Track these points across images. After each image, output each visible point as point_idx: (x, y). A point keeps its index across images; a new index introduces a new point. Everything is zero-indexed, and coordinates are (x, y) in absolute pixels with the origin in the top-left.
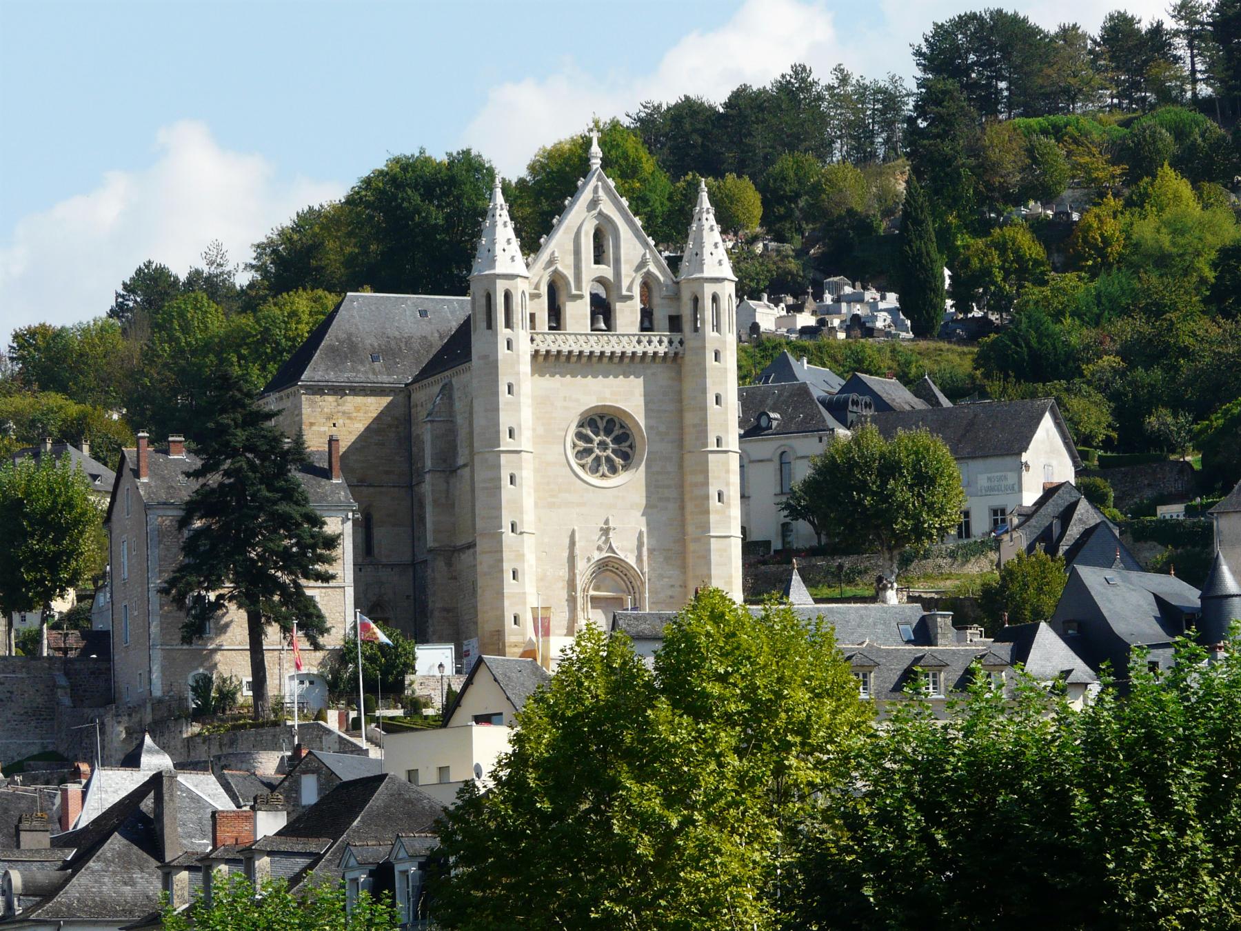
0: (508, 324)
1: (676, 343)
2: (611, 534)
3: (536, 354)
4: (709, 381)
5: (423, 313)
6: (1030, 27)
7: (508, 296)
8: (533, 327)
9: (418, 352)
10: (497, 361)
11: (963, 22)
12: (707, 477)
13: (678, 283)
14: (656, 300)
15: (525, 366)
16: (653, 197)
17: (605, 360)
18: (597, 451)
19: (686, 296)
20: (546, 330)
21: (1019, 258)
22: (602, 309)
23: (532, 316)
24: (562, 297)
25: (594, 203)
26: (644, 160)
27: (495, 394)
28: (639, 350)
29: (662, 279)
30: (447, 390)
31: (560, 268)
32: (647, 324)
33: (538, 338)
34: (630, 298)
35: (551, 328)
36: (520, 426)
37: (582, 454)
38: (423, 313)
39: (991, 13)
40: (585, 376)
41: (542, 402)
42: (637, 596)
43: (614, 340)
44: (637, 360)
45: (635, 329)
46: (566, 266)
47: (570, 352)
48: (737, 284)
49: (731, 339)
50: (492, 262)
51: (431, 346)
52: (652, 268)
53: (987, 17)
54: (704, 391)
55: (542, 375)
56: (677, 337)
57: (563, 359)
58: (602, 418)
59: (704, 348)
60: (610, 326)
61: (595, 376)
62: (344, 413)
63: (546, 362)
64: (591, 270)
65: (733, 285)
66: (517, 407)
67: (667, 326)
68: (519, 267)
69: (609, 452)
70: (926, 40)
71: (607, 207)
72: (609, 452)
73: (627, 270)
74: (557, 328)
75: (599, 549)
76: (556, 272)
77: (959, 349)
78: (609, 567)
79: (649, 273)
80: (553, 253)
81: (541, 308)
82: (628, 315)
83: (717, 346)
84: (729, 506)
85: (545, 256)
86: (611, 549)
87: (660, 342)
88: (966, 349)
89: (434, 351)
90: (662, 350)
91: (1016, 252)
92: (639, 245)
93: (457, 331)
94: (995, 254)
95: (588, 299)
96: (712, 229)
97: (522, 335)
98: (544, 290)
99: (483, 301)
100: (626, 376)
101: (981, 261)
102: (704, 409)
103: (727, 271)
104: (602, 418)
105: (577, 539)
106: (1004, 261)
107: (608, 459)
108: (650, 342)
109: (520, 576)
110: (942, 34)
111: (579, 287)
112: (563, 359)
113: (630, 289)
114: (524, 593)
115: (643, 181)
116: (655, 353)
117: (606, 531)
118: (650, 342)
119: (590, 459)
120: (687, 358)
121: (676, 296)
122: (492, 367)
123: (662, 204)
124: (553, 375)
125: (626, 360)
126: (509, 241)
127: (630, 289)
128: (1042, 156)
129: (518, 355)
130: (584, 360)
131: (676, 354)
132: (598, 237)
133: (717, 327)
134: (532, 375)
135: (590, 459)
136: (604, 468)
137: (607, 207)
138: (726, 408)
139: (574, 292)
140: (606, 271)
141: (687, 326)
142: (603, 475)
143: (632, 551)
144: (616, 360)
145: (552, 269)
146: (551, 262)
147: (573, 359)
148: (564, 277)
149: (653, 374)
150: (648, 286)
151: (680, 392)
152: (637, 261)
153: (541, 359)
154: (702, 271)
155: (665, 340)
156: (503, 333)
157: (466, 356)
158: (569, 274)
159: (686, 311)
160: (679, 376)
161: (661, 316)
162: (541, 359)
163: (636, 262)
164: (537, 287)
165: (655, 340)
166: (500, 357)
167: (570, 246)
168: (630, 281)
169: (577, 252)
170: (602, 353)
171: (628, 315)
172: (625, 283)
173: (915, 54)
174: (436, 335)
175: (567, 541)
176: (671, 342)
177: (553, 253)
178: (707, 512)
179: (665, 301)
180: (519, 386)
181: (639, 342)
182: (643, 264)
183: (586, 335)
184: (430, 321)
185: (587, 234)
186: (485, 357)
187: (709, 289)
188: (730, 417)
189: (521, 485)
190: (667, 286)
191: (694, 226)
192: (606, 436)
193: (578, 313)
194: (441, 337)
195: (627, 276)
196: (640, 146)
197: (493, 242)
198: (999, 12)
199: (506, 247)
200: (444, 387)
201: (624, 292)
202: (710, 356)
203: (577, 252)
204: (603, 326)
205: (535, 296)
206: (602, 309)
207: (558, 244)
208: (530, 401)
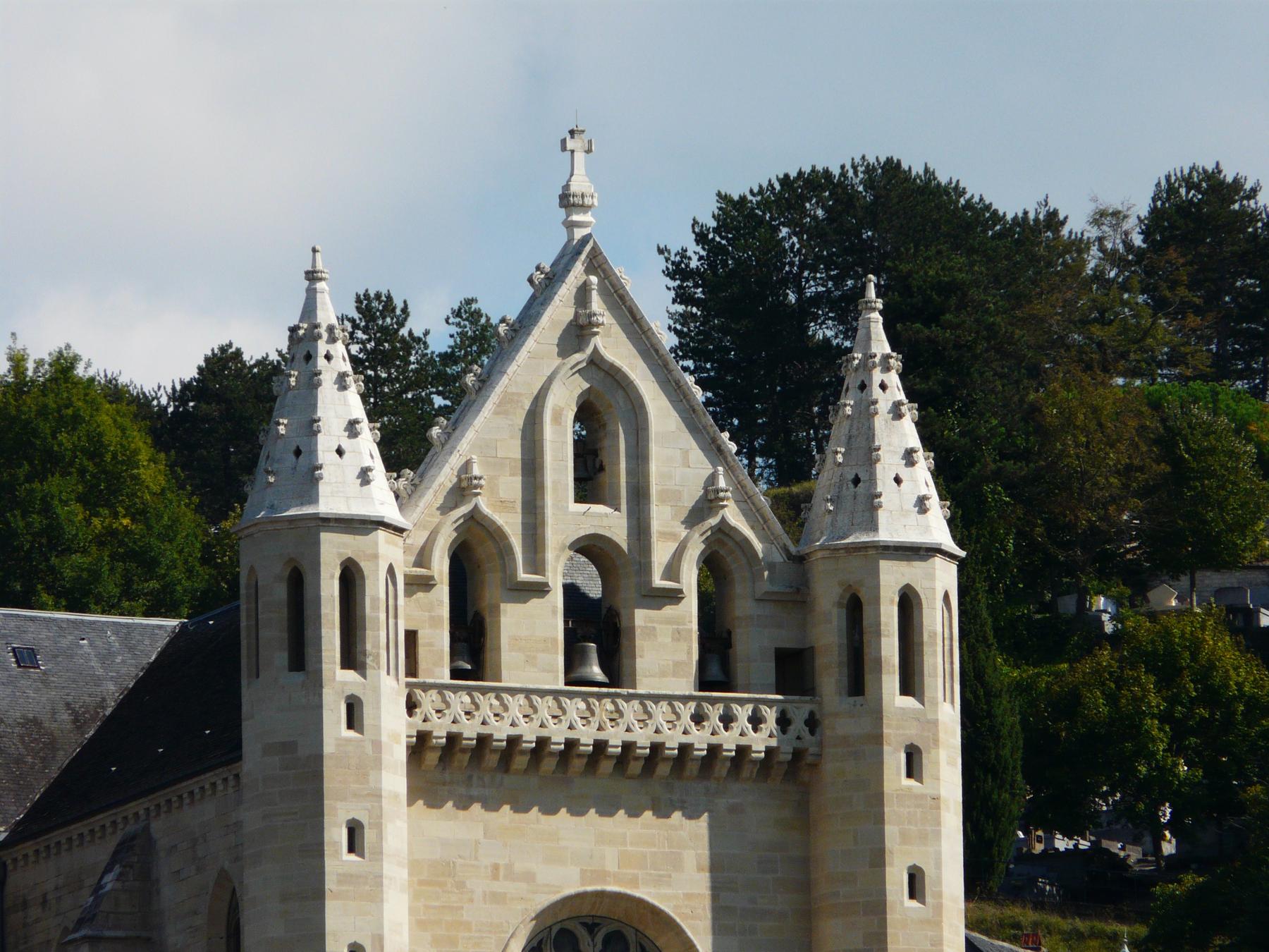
0: (352, 658)
1: (798, 726)
3: (419, 745)
4: (891, 831)
5: (26, 658)
6: (969, 205)
7: (351, 577)
8: (412, 670)
9: (19, 761)
10: (319, 758)
11: (796, 192)
13: (801, 559)
14: (743, 606)
15: (394, 779)
16: (170, 553)
17: (606, 766)
19: (827, 595)
20: (446, 678)
21: (1212, 695)
22: (597, 632)
23: (411, 637)
24: (491, 589)
26: (143, 457)
27: (315, 850)
28: (700, 739)
29: (758, 546)
30: (135, 854)
31: (486, 509)
32: (715, 671)
33: (428, 701)
34: (674, 596)
35: (456, 673)
38: (26, 658)
39: (869, 170)
40: (550, 810)
41: (434, 877)
43: (631, 710)
44: (692, 768)
45: (685, 684)
46: (503, 505)
47: (513, 741)
48: (962, 565)
49: (948, 715)
50: (309, 480)
51: (52, 745)
52: (733, 515)
53: (857, 182)
54: (878, 859)
55: (434, 802)
56: (800, 710)
57: (492, 760)
58: (591, 928)
59: (877, 739)
60: (617, 671)
61: (578, 811)
63: (452, 769)
64: (567, 518)
65: (953, 568)
66: (373, 888)
67: (772, 678)
68: (379, 499)
70: (701, 238)
73: (665, 520)
74: (477, 674)
76: (475, 520)
77: (1065, 924)
79: (724, 531)
80: (467, 466)
81: (433, 615)
82: (665, 645)
83: (912, 733)
85: (444, 476)
87: (756, 721)
88: (1081, 925)
89: (63, 759)
90: (760, 742)
91: (1204, 674)
92: (697, 455)
93: (121, 706)
94: (1149, 681)
95: (557, 598)
96: (896, 412)
97: (386, 691)
98: (440, 566)
99: (281, 592)
100: (662, 812)
101: (1112, 699)
102: (877, 907)
103: (936, 528)
104: (591, 928)
106: (1173, 701)
108: (727, 720)
110: (740, 221)
111: (536, 561)
112: (492, 760)
113: (672, 571)
115: (138, 514)
116: (742, 751)
118: (727, 720)
120: (829, 767)
121: (795, 593)
122: (305, 774)
123: (190, 572)
124: (463, 805)
125: (663, 769)
126: (352, 428)
127: (672, 571)
128: (1196, 455)
129: (377, 745)
130: (549, 764)
131: (798, 754)
132: (587, 413)
133: (910, 684)
134: (411, 802)
138: (939, 908)
139: (523, 576)
140: (609, 521)
141: (830, 680)
144: (635, 767)
145: (464, 509)
146: (463, 489)
147: (520, 762)
148: (496, 535)
149: (733, 809)
150: (719, 563)
151: (805, 863)
152: (692, 494)
153: (432, 758)
154: (873, 526)
155: (770, 715)
156: (338, 681)
157: (226, 747)
158: (511, 524)
159: (828, 635)
160: (803, 817)
161: (753, 645)
162: (432, 758)
163: (689, 501)
164: (422, 558)
165: (743, 713)
166: (329, 748)
167: (513, 450)
168: (674, 550)
169: (532, 467)
170: (600, 746)
171: (665, 645)
172: (661, 555)
173: (670, 275)
174: (65, 716)
176: (783, 722)
177: (467, 466)
180: (379, 826)
181: (698, 719)
182: (708, 503)
183: (556, 694)
184: (45, 680)
185: (557, 418)
186: (288, 747)
187: (892, 576)
188: (947, 934)
190: (771, 566)
191: (848, 405)
193: (530, 634)
194: (79, 723)
195: (665, 535)
196: (127, 422)
197: (311, 427)
198: (892, 167)
199: (346, 444)
200: (125, 847)
201: (658, 581)
202: (894, 761)
203: (532, 467)
204: (596, 671)
205: (418, 584)
206: (597, 632)
207: (482, 443)
208: (404, 874)
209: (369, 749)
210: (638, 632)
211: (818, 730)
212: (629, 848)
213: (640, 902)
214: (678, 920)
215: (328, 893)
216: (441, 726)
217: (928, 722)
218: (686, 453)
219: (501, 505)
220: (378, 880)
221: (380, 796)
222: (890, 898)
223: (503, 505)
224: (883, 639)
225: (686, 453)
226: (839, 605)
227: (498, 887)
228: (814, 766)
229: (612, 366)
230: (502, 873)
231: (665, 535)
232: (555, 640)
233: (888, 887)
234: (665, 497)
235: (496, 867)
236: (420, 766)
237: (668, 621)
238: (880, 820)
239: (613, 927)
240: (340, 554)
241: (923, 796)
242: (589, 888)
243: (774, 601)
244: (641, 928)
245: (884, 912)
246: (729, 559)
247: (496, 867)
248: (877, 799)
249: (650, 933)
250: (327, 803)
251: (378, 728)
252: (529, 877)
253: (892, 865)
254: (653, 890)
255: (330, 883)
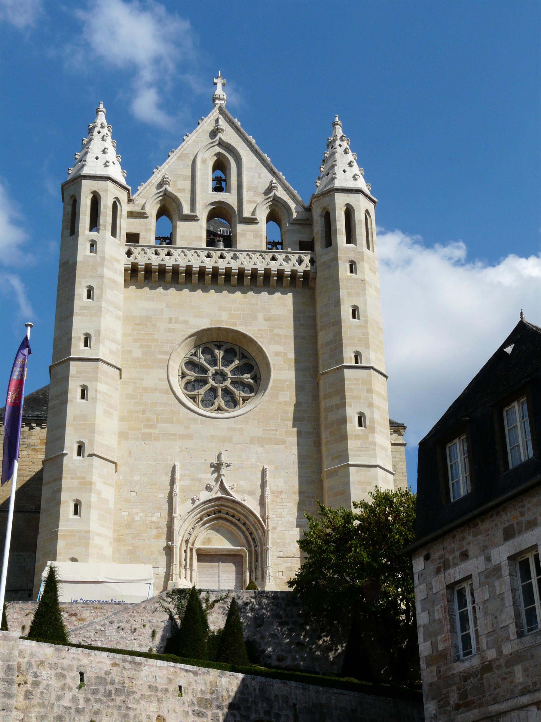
0: (350, 238)
2: (223, 472)
4: (343, 293)
12: (343, 398)
18: (212, 382)
25: (214, 133)
31: (170, 189)
36: (98, 332)
37: (190, 386)
41: (141, 324)
42: (259, 549)
52: (281, 193)
54: (337, 303)
62: (29, 445)
63: (136, 275)
69: (228, 383)
71: (229, 136)
72: (228, 383)
75: (209, 488)
78: (224, 512)
82: (253, 237)
83: (352, 257)
84: (373, 430)
85: (156, 179)
86: (222, 488)
102: (338, 322)
105: (177, 475)
107: (226, 391)
109: (83, 509)
114: (88, 532)
117: (217, 468)
119: (202, 391)
132: (220, 165)
135: (202, 391)
136: (220, 401)
137: (229, 136)
138: (366, 321)
142: (219, 409)
143: (251, 493)
165: (281, 257)
166: (80, 258)
168: (255, 205)
171: (253, 237)
175: (167, 480)
178: (344, 438)
179: (296, 227)
180: (101, 289)
182: (270, 189)
189: (95, 399)
192: (225, 366)
195: (249, 202)
209: (99, 259)
210: (238, 235)
211: (315, 265)
212: (233, 312)
213: (237, 332)
214: (254, 339)
215: (298, 493)
216: (142, 261)
217: (359, 252)
218: (260, 175)
219: (180, 189)
220: (100, 308)
221: (103, 277)
222: (343, 317)
223: (182, 191)
224: (337, 222)
225: (260, 175)
226: (321, 216)
227: (171, 326)
228: (315, 279)
229: (227, 143)
230: (173, 321)
231: (249, 202)
232: (201, 238)
233: (342, 313)
234: (249, 189)
235: (171, 319)
236: (137, 281)
237: (251, 231)
238: (338, 288)
239: (251, 362)
240: (90, 189)
241: (357, 279)
242: (213, 326)
243: (298, 224)
244: (241, 346)
245: (341, 323)
246: (280, 212)
247: (171, 319)
248: (336, 281)
249: (245, 347)
250: (77, 279)
251: (104, 252)
252: (186, 322)
253: (344, 305)
254: (243, 328)
255: (76, 309)
